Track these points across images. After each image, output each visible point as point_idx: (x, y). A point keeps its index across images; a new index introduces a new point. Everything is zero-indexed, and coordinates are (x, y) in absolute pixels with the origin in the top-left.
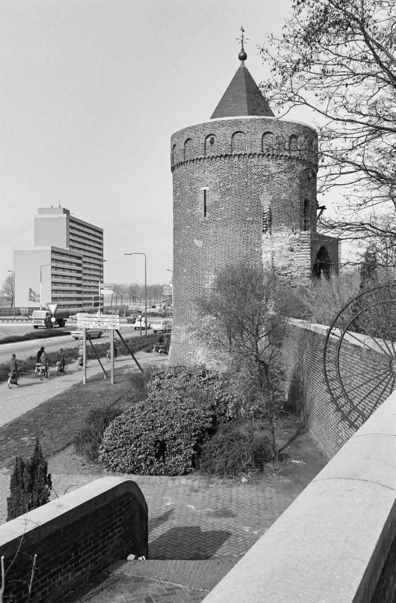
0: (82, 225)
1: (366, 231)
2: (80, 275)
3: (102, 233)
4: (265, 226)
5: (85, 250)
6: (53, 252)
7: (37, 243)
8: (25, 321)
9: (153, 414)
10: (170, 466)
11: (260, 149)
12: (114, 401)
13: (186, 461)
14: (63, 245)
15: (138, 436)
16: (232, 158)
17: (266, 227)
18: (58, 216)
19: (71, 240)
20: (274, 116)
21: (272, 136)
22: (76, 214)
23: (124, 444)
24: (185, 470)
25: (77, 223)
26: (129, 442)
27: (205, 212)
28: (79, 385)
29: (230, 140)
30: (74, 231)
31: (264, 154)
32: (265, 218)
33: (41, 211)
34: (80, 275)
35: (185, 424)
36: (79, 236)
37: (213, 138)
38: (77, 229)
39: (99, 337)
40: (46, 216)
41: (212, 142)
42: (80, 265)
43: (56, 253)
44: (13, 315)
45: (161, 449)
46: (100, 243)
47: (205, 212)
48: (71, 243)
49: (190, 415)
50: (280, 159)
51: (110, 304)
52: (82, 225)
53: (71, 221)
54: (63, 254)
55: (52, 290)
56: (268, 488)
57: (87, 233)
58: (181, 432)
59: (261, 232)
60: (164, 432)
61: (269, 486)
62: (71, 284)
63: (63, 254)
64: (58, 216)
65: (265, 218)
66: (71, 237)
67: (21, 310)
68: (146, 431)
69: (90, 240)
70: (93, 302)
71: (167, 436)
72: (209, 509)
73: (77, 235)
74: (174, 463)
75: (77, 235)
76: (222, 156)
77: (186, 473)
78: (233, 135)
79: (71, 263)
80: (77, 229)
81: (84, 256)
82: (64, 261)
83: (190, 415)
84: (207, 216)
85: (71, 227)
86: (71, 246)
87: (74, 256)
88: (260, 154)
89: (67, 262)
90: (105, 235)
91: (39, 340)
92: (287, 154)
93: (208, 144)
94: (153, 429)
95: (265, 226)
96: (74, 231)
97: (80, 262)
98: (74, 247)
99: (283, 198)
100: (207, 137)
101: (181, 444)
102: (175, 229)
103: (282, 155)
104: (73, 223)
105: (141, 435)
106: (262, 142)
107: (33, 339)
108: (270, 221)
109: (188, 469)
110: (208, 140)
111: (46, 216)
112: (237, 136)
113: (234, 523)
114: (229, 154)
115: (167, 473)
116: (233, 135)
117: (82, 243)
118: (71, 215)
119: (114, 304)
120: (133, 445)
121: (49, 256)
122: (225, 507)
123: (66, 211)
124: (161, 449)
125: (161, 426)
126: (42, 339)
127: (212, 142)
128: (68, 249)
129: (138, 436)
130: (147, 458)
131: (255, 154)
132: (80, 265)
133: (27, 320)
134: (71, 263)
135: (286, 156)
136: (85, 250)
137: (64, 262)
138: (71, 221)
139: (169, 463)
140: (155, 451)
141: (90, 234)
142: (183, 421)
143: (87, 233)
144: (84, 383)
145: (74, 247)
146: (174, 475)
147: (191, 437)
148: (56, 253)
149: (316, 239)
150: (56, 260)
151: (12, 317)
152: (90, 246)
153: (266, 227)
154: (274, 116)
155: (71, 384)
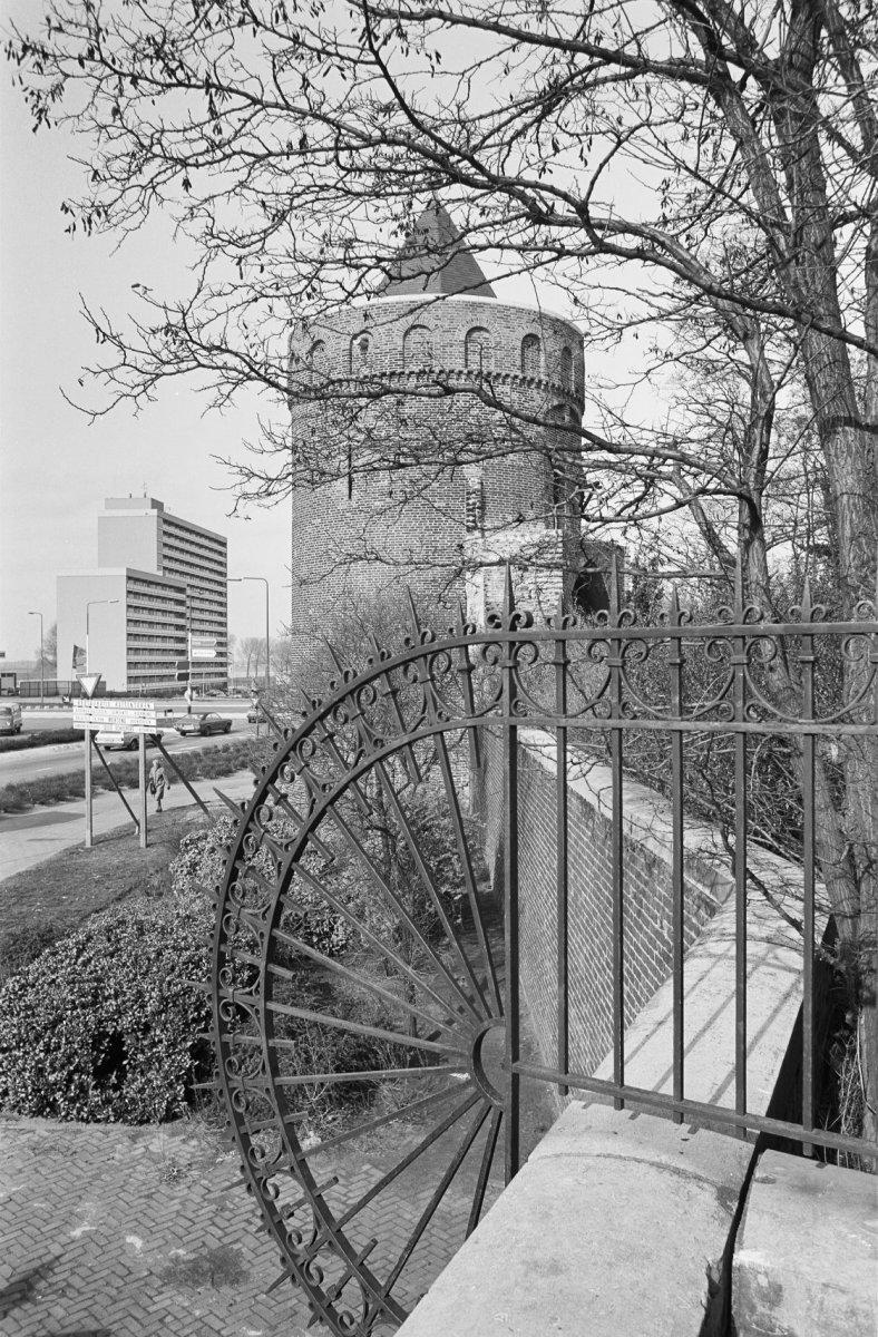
0: (187, 530)
1: (235, 237)
2: (181, 621)
3: (224, 544)
4: (471, 518)
5: (192, 576)
6: (129, 578)
7: (102, 563)
8: (56, 708)
9: (104, 962)
10: (133, 1099)
11: (462, 361)
12: (119, 892)
13: (171, 1085)
14: (150, 565)
15: (54, 1024)
16: (404, 378)
17: (474, 521)
18: (142, 512)
19: (165, 557)
20: (493, 296)
21: (486, 335)
22: (175, 510)
23: (21, 1041)
24: (168, 1109)
25: (177, 526)
26: (32, 1037)
27: (350, 490)
28: (73, 852)
29: (400, 342)
30: (171, 541)
31: (470, 373)
32: (471, 502)
33: (111, 503)
34: (181, 621)
35: (175, 989)
36: (182, 551)
37: (367, 340)
38: (177, 537)
39: (226, 731)
40: (121, 513)
41: (364, 347)
42: (181, 603)
43: (137, 580)
44: (39, 696)
45: (110, 1058)
46: (221, 563)
47: (350, 490)
48: (167, 563)
49: (191, 966)
50: (504, 383)
51: (243, 675)
52: (187, 530)
53: (165, 521)
54: (150, 583)
55: (129, 649)
56: (366, 1167)
57: (197, 544)
58: (163, 1011)
59: (464, 531)
60: (120, 1012)
61: (369, 1161)
62: (164, 638)
63: (150, 583)
64: (142, 512)
65: (471, 502)
66: (167, 552)
67: (59, 685)
68: (75, 1008)
69: (202, 557)
70: (176, 672)
71: (126, 1022)
72: (181, 1252)
73: (177, 549)
74: (141, 1091)
75: (206, 548)
76: (384, 374)
77: (170, 1116)
78: (407, 333)
79: (164, 599)
80: (177, 537)
81: (192, 587)
82: (151, 596)
83: (191, 966)
84: (354, 498)
85: (165, 533)
86: (165, 568)
87: (171, 587)
88: (461, 372)
89: (158, 597)
90: (230, 550)
91: (56, 747)
92: (518, 373)
93: (357, 350)
94: (94, 1003)
95: (471, 518)
96: (171, 541)
97: (181, 596)
98: (171, 570)
99: (509, 462)
100: (355, 337)
101: (161, 1041)
102: (295, 525)
103: (507, 376)
104: (171, 527)
105: (60, 1019)
106: (466, 349)
107: (45, 744)
108: (482, 508)
109: (178, 1107)
110: (356, 342)
111: (121, 513)
112: (415, 336)
113: (222, 1313)
114: (399, 371)
115: (121, 1115)
116: (407, 333)
117: (187, 563)
118: (166, 510)
119: (252, 674)
120: (41, 1045)
121: (123, 586)
122: (226, 1240)
123: (157, 505)
124: (110, 1058)
125: (116, 996)
126: (62, 746)
127: (364, 347)
128: (160, 573)
129: (54, 1024)
130: (70, 1080)
131: (452, 371)
132: (181, 603)
133: (60, 705)
134: (164, 599)
135: (516, 377)
136: (192, 576)
137: (151, 596)
138: (165, 521)
139: (130, 1091)
140: (94, 1062)
141: (201, 546)
142: (169, 983)
143: (197, 544)
144: (88, 845)
145: (171, 570)
146: (141, 1123)
147: (187, 1025)
148: (137, 580)
149: (578, 546)
150: (136, 594)
151: (38, 700)
152: (202, 568)
153: (474, 521)
154: (493, 296)
155: (60, 847)
